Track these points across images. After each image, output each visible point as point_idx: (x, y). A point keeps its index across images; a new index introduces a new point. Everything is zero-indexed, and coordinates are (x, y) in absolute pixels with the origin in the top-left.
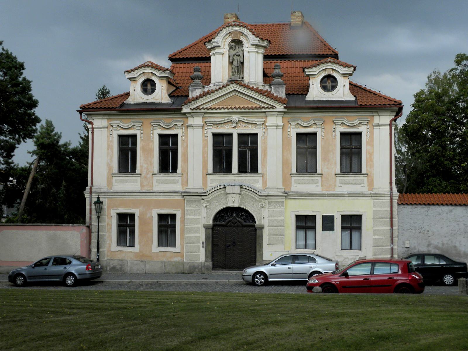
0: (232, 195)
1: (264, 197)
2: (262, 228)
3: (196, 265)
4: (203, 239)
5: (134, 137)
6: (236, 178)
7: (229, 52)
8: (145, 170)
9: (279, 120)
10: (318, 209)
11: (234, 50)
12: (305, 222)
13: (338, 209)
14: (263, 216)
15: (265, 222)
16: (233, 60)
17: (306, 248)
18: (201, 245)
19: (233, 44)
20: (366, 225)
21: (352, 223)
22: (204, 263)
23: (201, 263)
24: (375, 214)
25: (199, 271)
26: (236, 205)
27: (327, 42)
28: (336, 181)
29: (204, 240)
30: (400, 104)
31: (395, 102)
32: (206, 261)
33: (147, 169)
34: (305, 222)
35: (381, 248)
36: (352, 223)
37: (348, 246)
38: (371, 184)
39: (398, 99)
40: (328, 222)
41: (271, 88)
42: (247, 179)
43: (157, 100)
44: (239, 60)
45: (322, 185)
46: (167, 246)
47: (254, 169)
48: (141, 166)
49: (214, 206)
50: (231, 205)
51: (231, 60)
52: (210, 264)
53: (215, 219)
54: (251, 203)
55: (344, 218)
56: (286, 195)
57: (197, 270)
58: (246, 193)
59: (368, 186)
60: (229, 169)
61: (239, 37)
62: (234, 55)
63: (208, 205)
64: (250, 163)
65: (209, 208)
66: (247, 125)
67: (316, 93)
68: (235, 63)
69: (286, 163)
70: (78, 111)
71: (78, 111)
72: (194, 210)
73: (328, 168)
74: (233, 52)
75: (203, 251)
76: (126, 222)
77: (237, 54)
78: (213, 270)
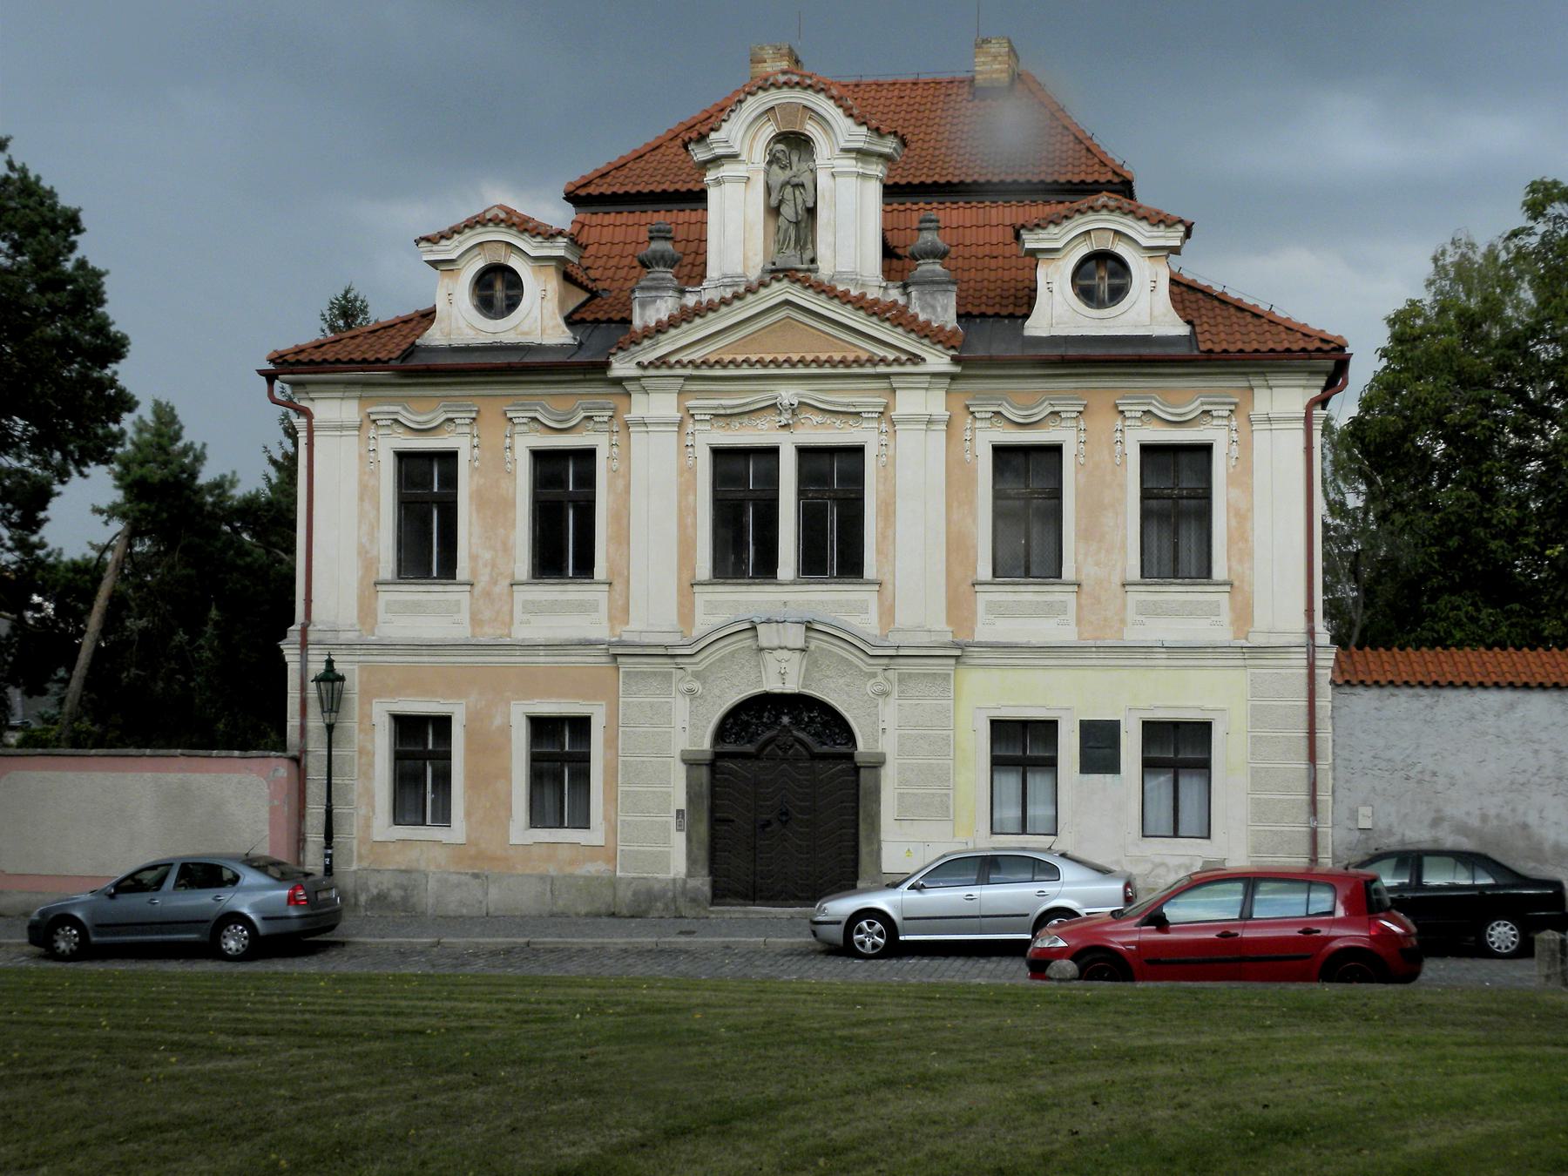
0: (779, 654)
1: (886, 661)
2: (877, 764)
3: (657, 887)
4: (680, 800)
5: (450, 457)
6: (789, 595)
7: (767, 173)
8: (488, 570)
9: (934, 402)
10: (1066, 699)
11: (783, 168)
12: (1021, 746)
13: (1133, 699)
14: (881, 724)
15: (888, 745)
16: (781, 202)
17: (1024, 831)
18: (673, 821)
19: (781, 147)
20: (1226, 752)
21: (1179, 748)
22: (685, 882)
23: (674, 880)
24: (1258, 715)
25: (666, 908)
26: (791, 687)
27: (1096, 141)
28: (1124, 606)
29: (682, 805)
30: (1341, 348)
31: (1323, 340)
32: (690, 874)
33: (494, 566)
34: (1021, 746)
35: (1275, 833)
36: (1179, 748)
37: (1166, 824)
38: (1243, 615)
39: (1332, 331)
40: (1100, 745)
41: (908, 295)
42: (828, 599)
43: (523, 333)
44: (799, 201)
45: (1079, 621)
46: (561, 826)
47: (851, 567)
48: (474, 558)
49: (717, 692)
50: (774, 686)
51: (774, 202)
52: (702, 883)
53: (721, 733)
54: (841, 681)
55: (1152, 730)
56: (960, 653)
57: (660, 905)
58: (825, 646)
59: (1232, 624)
60: (767, 568)
61: (802, 123)
62: (784, 185)
63: (696, 685)
64: (836, 548)
65: (701, 697)
66: (829, 419)
67: (1057, 311)
68: (788, 211)
69: (957, 546)
70: (261, 372)
71: (261, 372)
72: (652, 705)
73: (1097, 564)
74: (780, 176)
75: (679, 841)
76: (421, 746)
77: (795, 180)
78: (712, 904)
